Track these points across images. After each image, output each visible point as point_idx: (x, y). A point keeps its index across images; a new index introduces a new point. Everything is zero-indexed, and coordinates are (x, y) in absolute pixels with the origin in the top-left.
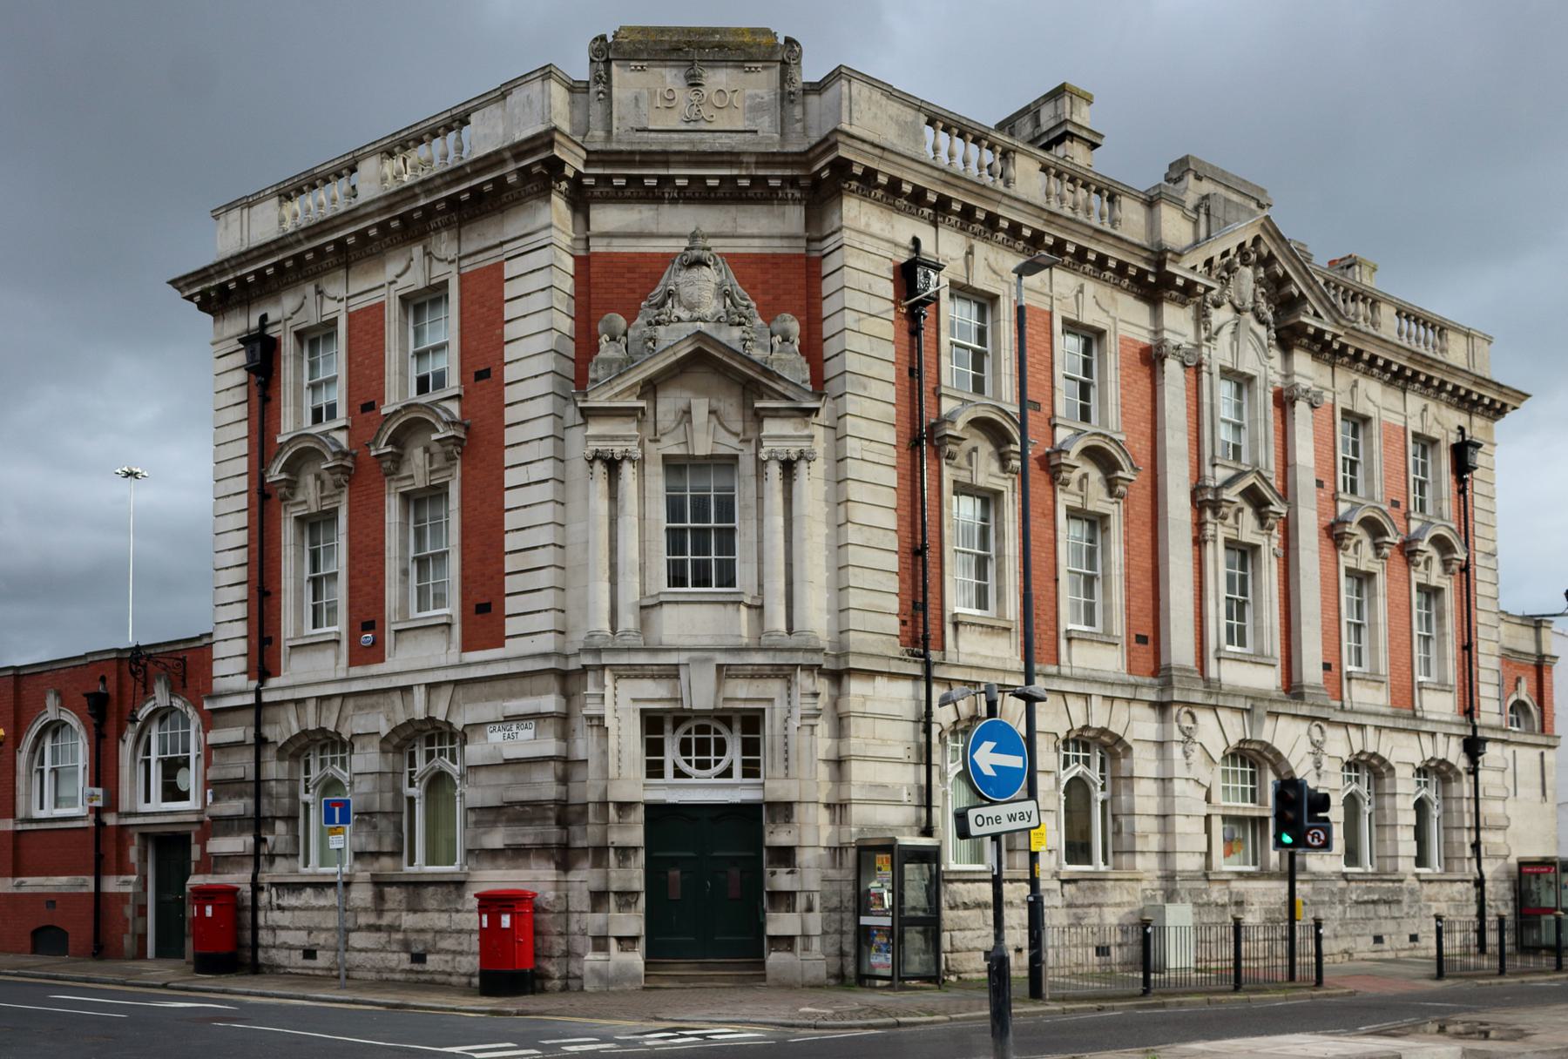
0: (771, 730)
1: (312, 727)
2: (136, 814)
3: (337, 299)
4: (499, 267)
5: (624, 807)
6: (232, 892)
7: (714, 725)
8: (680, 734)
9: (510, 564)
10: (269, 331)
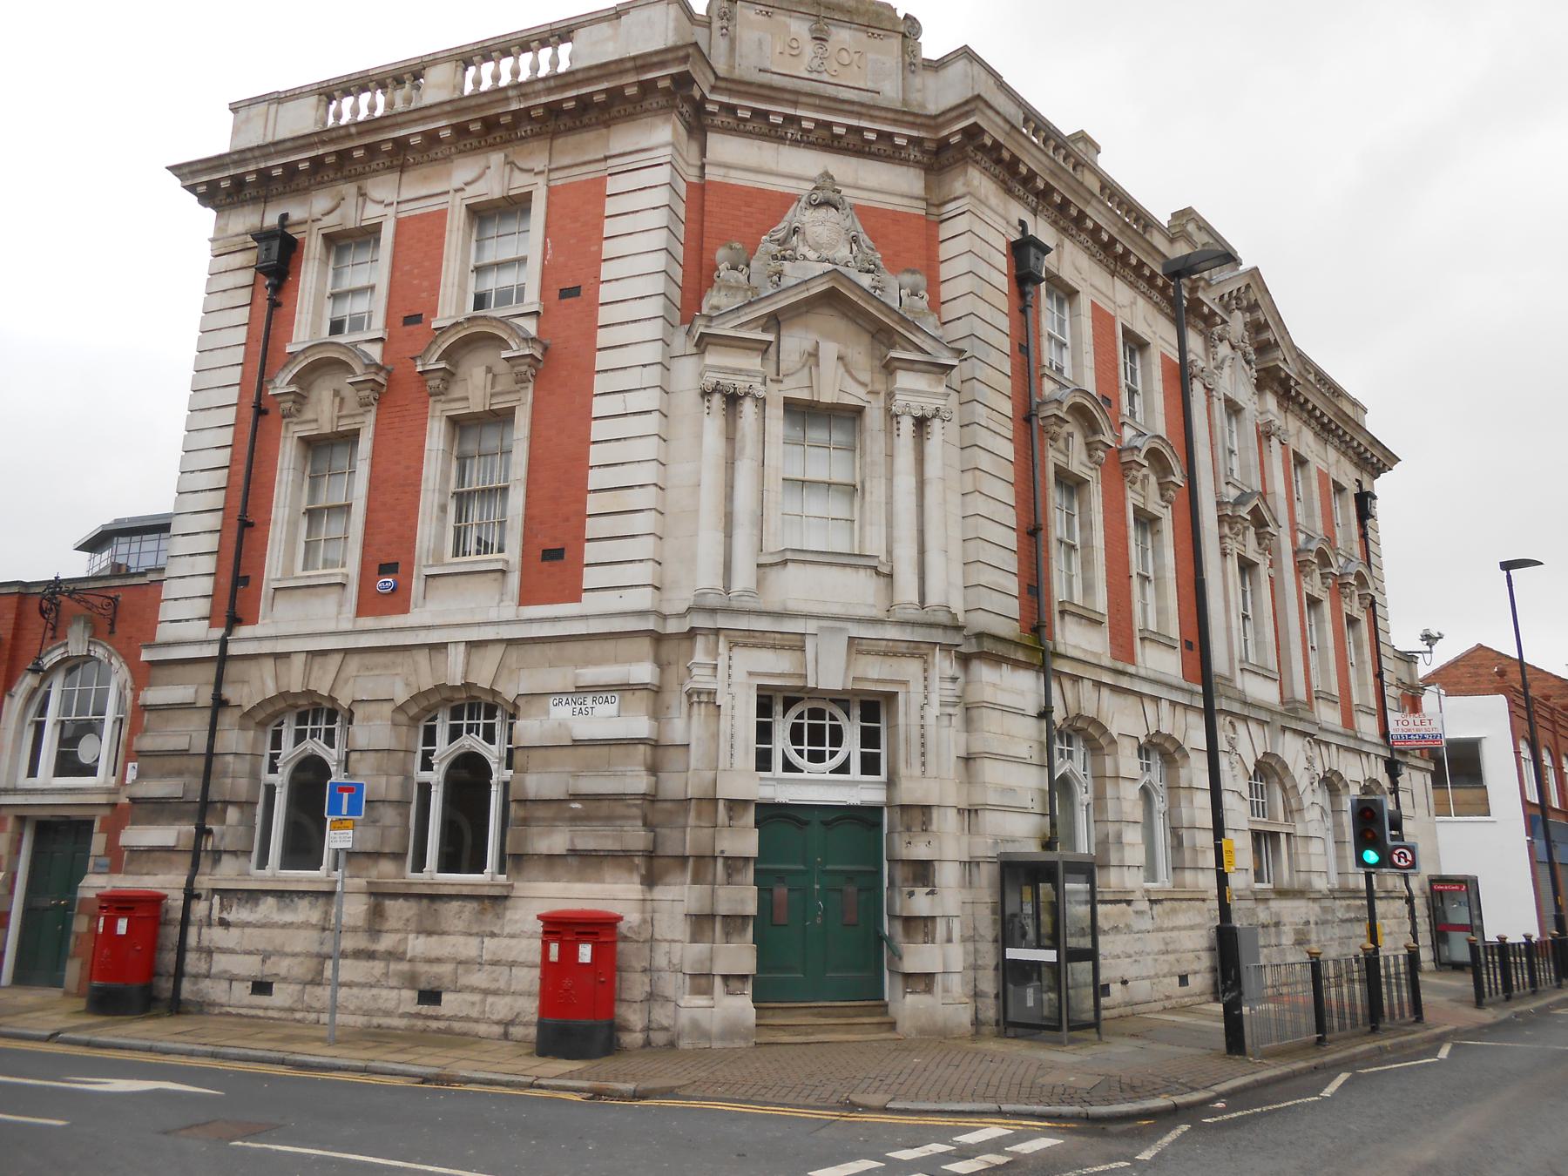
0: (906, 715)
2: (15, 791)
3: (385, 201)
4: (601, 182)
5: (735, 805)
7: (830, 709)
9: (593, 504)
10: (289, 231)
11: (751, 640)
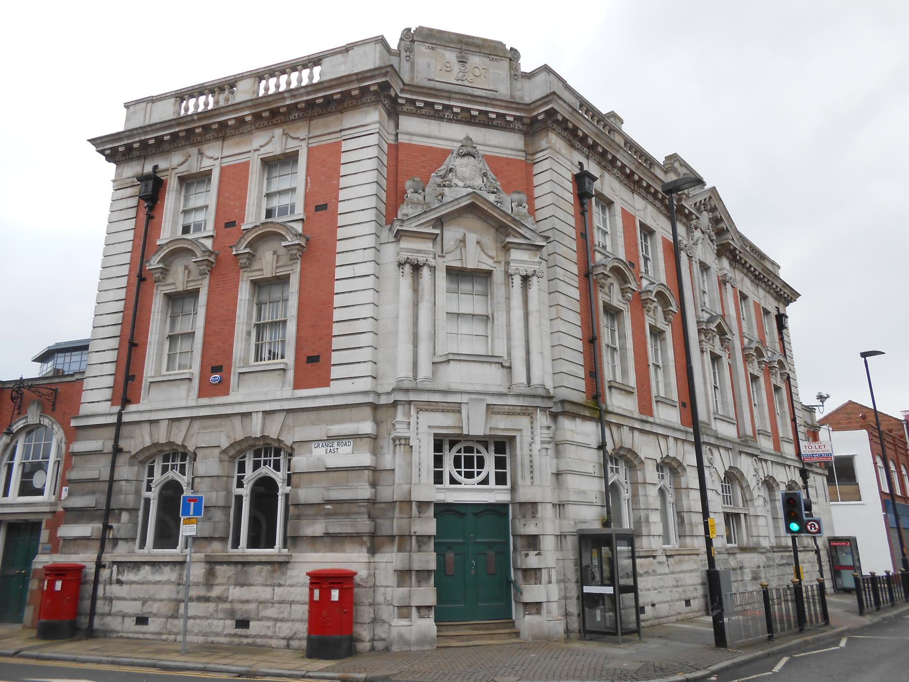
0: (521, 449)
1: (163, 441)
3: (214, 157)
4: (338, 144)
6: (78, 570)
7: (477, 447)
8: (454, 452)
9: (336, 329)
10: (159, 175)
11: (431, 407)
